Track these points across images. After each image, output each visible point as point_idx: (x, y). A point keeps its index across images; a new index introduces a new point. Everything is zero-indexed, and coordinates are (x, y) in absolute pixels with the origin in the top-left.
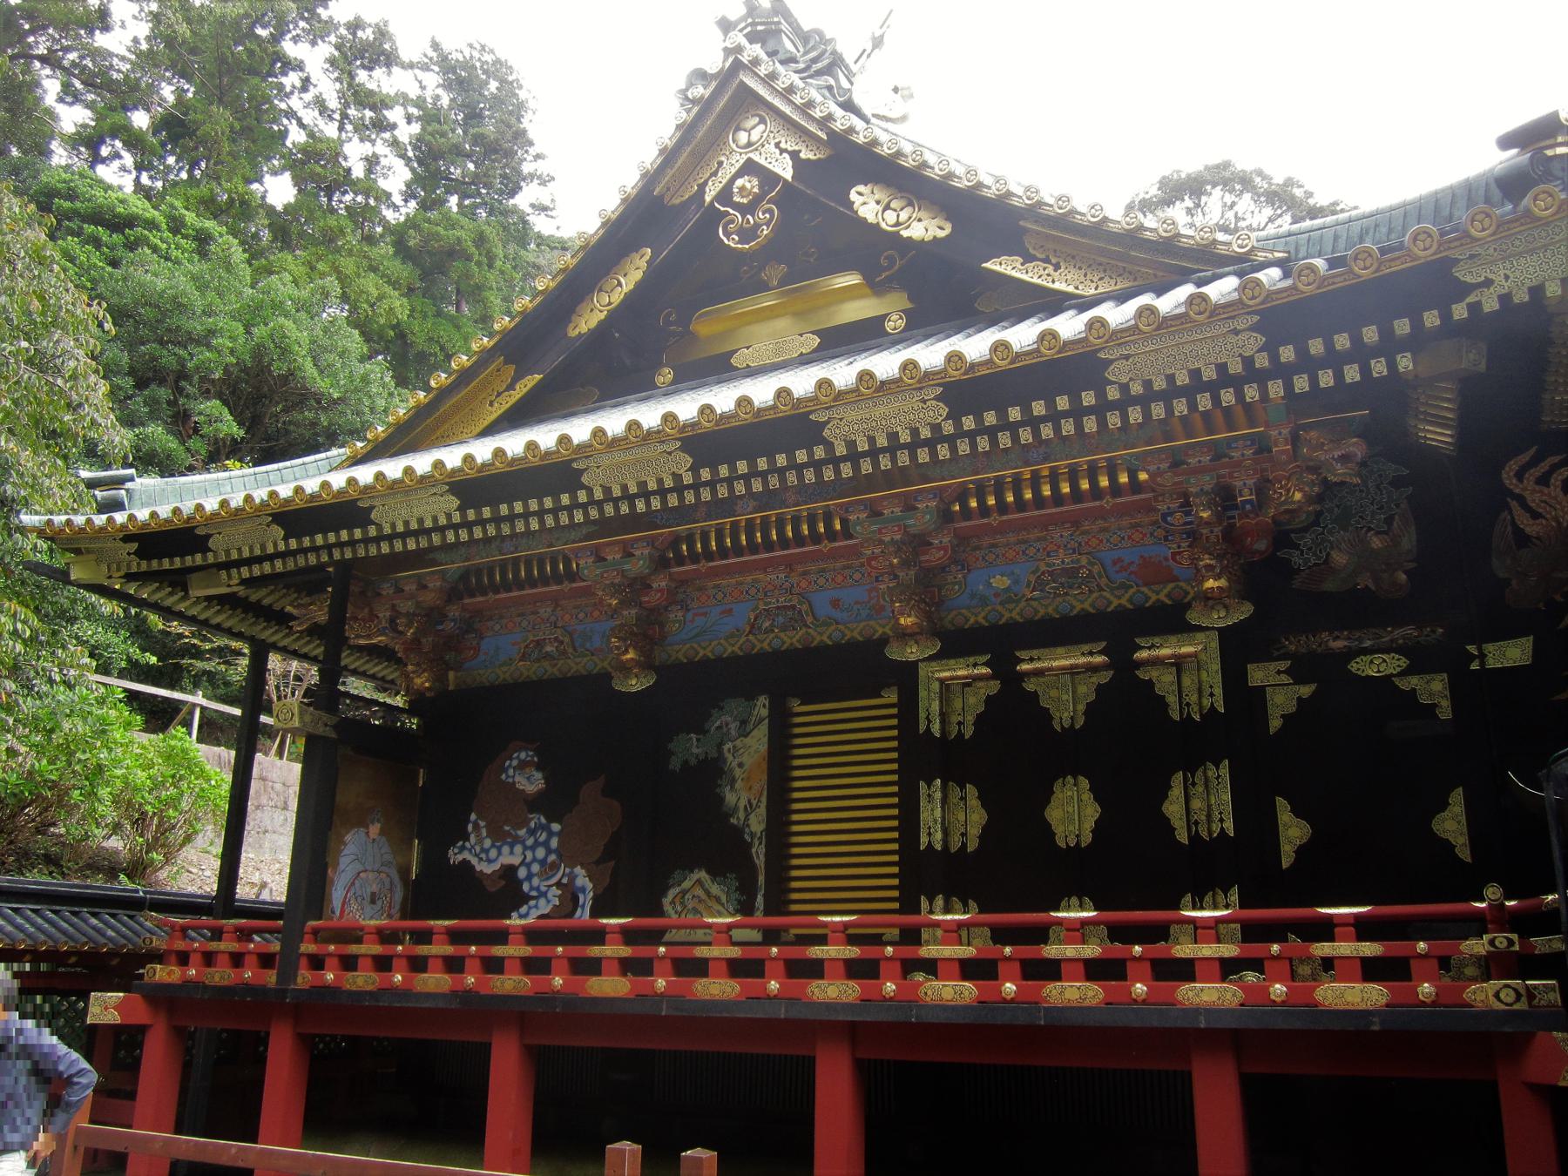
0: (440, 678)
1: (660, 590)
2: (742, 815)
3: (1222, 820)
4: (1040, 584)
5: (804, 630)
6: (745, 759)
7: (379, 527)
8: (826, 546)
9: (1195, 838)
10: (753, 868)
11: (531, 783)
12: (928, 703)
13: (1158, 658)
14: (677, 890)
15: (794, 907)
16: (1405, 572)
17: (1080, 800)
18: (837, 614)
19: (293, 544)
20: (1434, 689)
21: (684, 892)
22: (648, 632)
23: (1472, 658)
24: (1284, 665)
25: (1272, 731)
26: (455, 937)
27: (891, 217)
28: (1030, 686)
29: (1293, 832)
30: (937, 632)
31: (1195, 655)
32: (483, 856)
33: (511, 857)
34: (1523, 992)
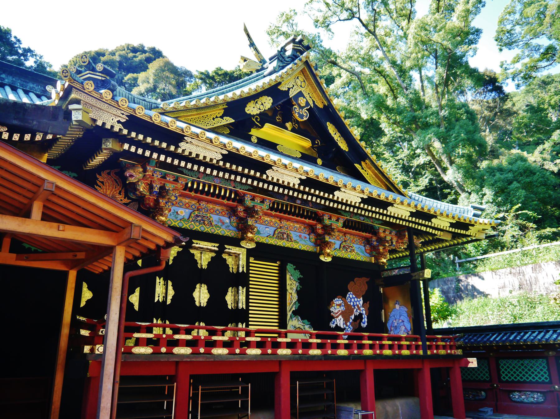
3: (159, 297)
7: (267, 177)
8: (193, 194)
19: (362, 205)
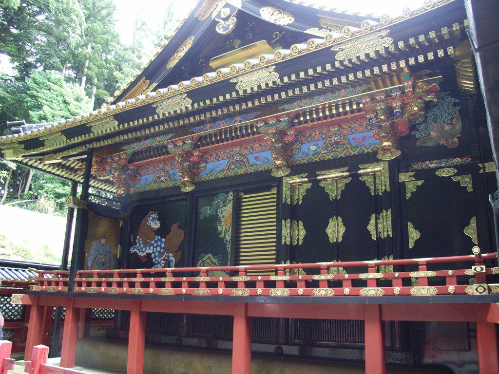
0: (128, 190)
1: (196, 156)
2: (223, 234)
3: (388, 231)
4: (326, 148)
5: (245, 168)
6: (225, 214)
8: (251, 137)
9: (379, 238)
10: (226, 253)
11: (156, 225)
12: (286, 192)
13: (367, 172)
14: (202, 260)
15: (241, 262)
16: (457, 138)
17: (338, 225)
18: (256, 162)
20: (466, 181)
21: (204, 261)
22: (193, 171)
23: (480, 168)
24: (413, 173)
25: (407, 198)
26: (100, 275)
27: (274, 18)
28: (322, 185)
29: (414, 235)
30: (288, 166)
31: (380, 171)
32: (141, 250)
33: (149, 251)
34: (486, 288)
